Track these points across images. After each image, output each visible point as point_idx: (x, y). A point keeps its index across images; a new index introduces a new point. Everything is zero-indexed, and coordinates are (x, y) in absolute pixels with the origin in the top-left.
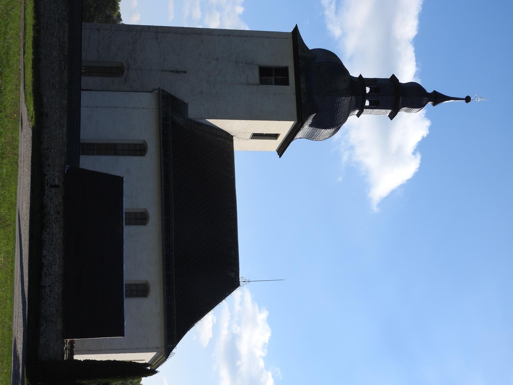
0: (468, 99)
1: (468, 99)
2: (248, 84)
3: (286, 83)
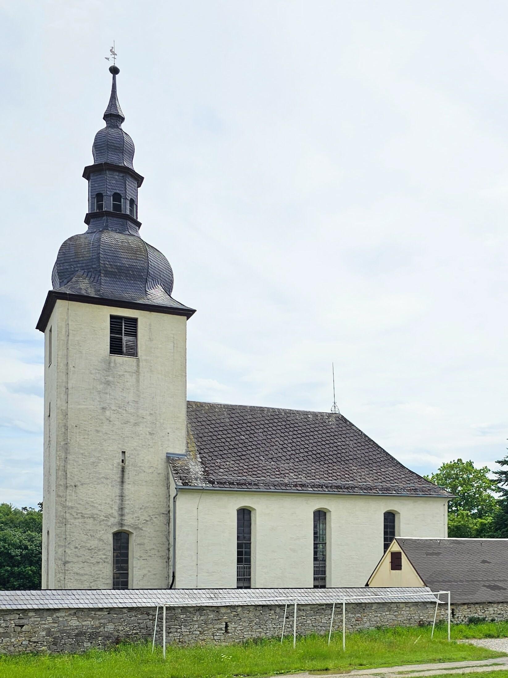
0: (114, 71)
1: (114, 71)
2: (138, 372)
3: (133, 322)
